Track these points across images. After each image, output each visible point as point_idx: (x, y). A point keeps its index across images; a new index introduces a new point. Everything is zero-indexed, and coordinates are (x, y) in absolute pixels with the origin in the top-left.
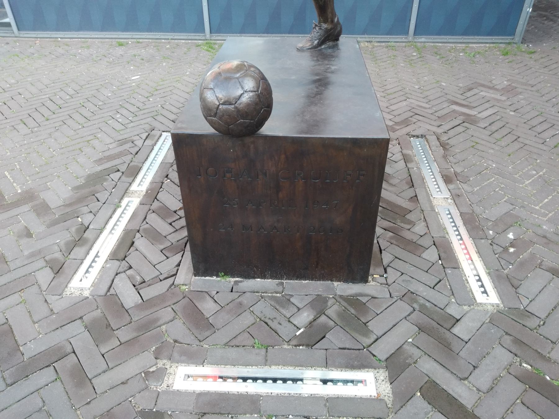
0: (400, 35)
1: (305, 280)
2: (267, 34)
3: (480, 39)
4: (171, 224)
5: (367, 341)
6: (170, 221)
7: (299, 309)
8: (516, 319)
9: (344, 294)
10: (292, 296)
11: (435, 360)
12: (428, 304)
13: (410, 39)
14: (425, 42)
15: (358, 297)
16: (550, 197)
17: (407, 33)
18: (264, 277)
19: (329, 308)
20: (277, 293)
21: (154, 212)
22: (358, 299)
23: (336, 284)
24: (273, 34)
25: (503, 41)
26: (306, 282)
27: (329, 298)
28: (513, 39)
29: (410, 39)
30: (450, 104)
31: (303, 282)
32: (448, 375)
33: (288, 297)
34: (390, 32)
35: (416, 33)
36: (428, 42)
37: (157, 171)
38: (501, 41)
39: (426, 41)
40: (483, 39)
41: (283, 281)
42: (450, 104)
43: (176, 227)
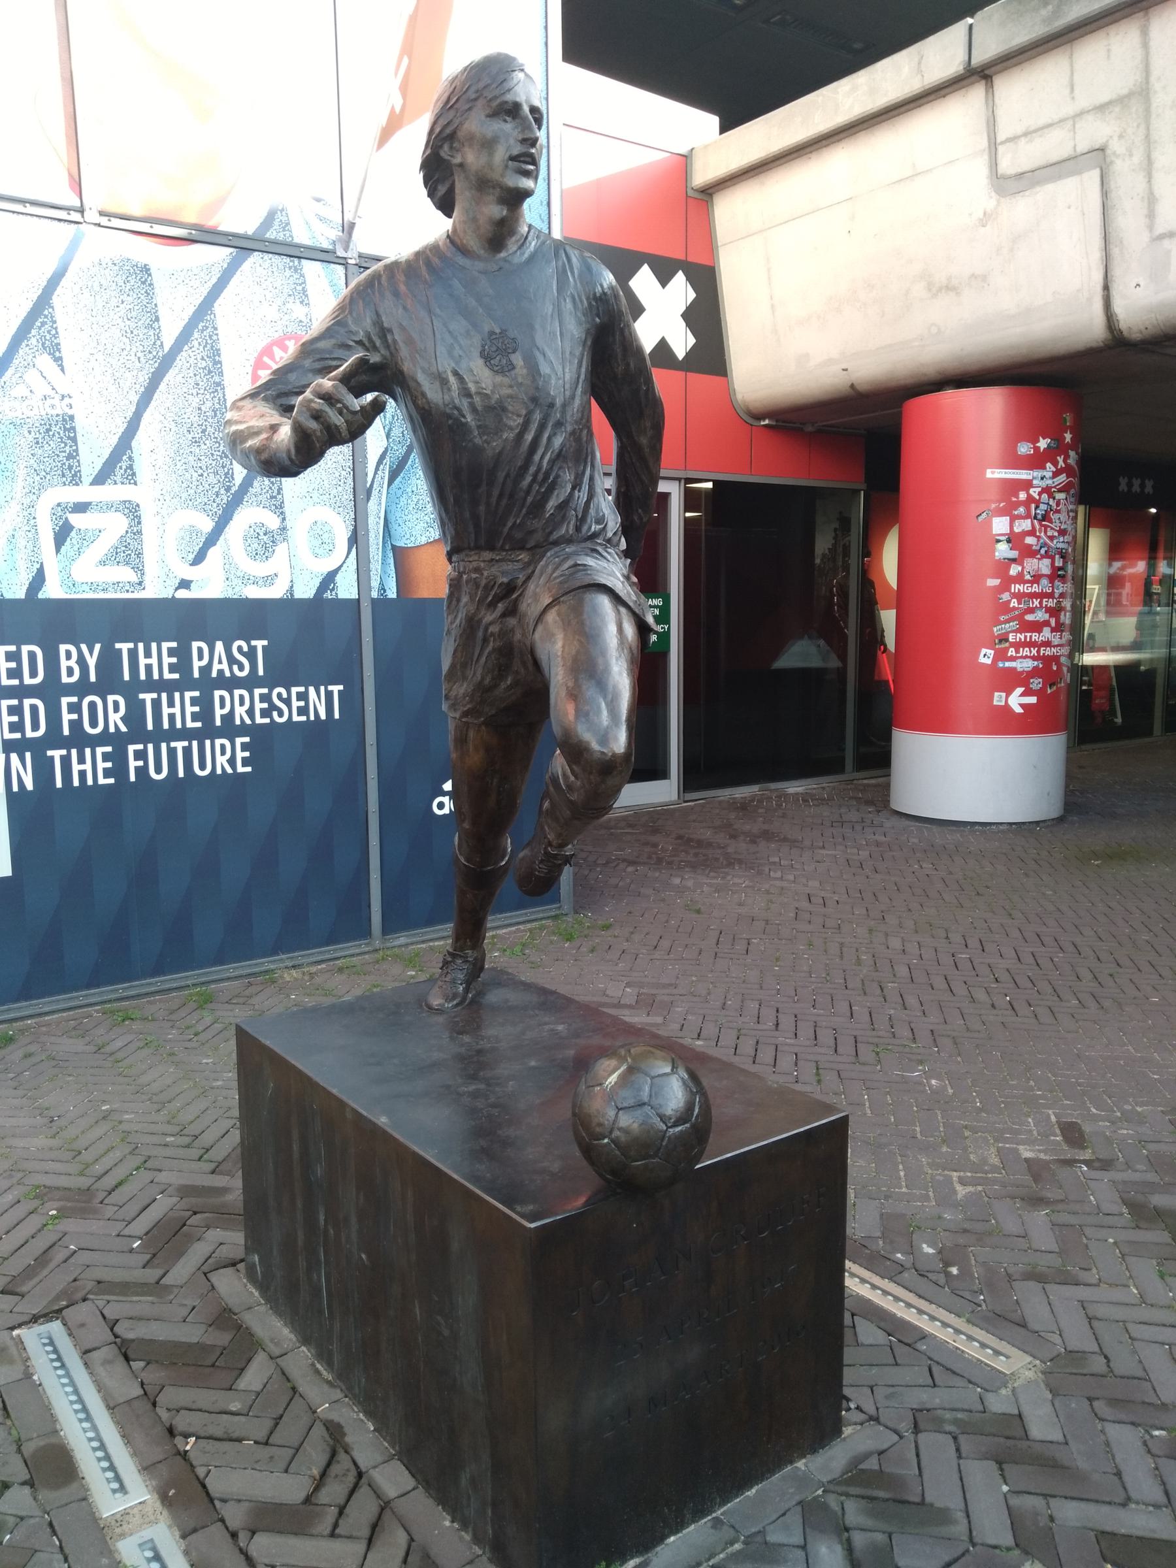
0: (355, 939)
1: (752, 1487)
2: (26, 1001)
3: (505, 918)
4: (332, 1535)
5: (960, 1529)
6: (325, 1526)
7: (804, 1547)
8: (1074, 1371)
9: (836, 1474)
10: (762, 1532)
11: (1066, 1498)
12: (960, 1415)
13: (377, 943)
14: (407, 945)
15: (862, 1466)
16: (901, 1167)
17: (366, 933)
18: (678, 1526)
19: (843, 1515)
20: (732, 1544)
21: (254, 1533)
22: (862, 1470)
23: (801, 1464)
24: (43, 997)
25: (546, 915)
26: (754, 1491)
27: (819, 1496)
28: (559, 908)
29: (377, 943)
30: (94, 1187)
31: (749, 1493)
32: (1105, 1509)
33: (759, 1539)
34: (332, 938)
35: (386, 930)
36: (412, 944)
37: (123, 1436)
38: (541, 915)
39: (409, 941)
40: (511, 917)
41: (714, 1515)
42: (94, 1187)
43: (359, 1534)
